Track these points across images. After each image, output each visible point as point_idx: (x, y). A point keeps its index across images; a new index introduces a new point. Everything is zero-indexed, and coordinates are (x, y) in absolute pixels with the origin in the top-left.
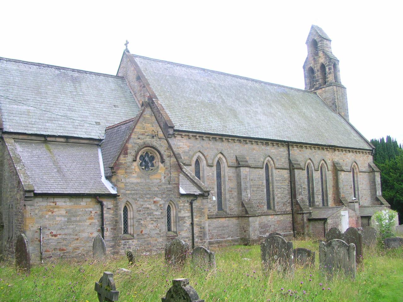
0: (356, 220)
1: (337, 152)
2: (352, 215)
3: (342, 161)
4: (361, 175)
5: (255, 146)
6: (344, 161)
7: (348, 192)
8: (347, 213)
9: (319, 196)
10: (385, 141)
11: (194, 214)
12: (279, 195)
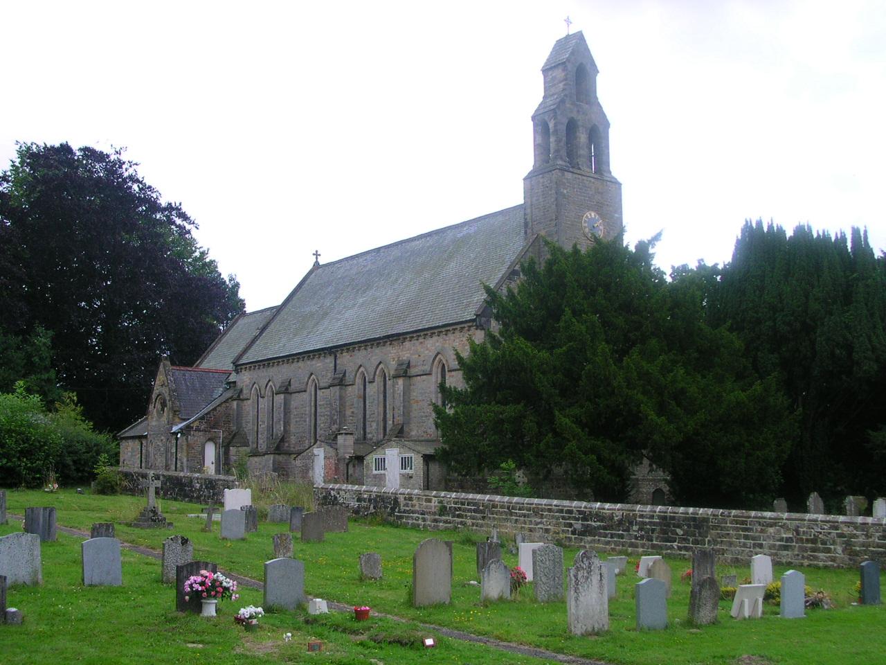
0: (335, 464)
1: (407, 344)
2: (330, 455)
3: (417, 356)
4: (453, 376)
5: (301, 364)
6: (419, 356)
7: (424, 412)
8: (323, 451)
9: (372, 423)
10: (754, 225)
11: (178, 450)
12: (322, 425)
